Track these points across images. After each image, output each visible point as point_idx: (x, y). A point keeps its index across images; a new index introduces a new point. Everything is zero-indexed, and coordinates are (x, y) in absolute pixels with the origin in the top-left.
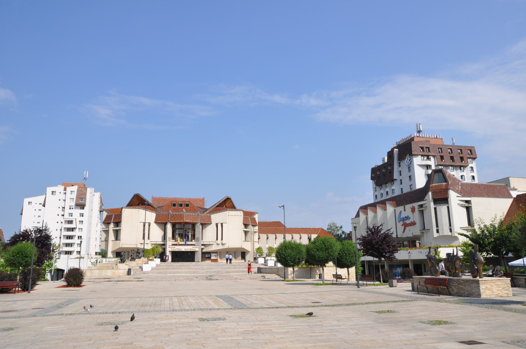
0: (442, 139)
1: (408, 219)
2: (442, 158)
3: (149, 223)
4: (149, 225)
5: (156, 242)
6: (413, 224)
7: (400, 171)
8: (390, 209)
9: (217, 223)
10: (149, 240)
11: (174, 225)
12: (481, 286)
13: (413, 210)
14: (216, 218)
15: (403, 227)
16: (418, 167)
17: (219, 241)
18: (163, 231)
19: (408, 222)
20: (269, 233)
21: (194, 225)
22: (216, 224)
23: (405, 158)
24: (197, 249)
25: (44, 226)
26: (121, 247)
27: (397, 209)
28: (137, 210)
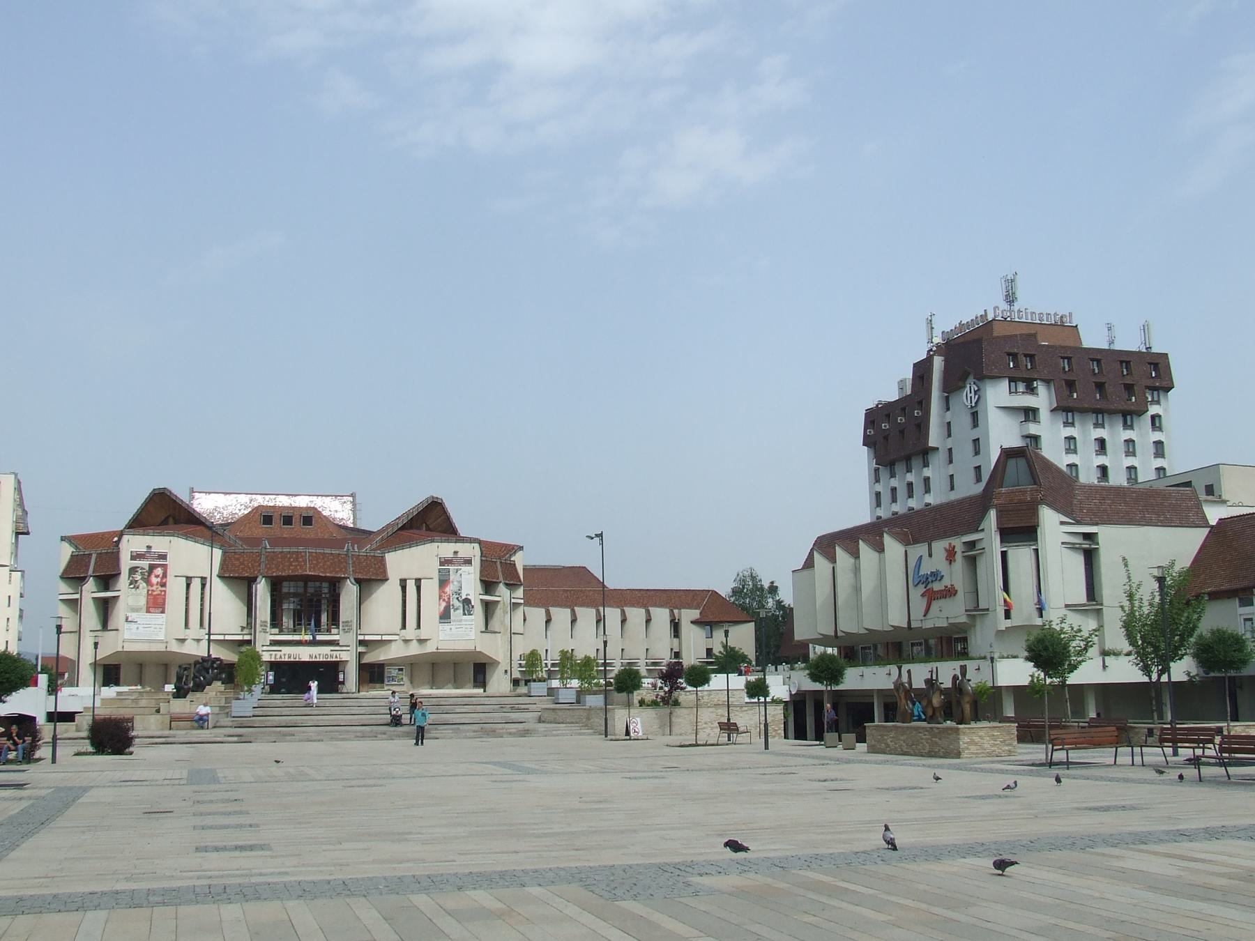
0: (1076, 326)
1: (939, 578)
2: (1071, 385)
3: (202, 578)
4: (203, 586)
5: (382, 635)
6: (950, 592)
7: (949, 424)
8: (893, 547)
9: (403, 577)
11: (276, 585)
12: (961, 737)
13: (951, 555)
14: (401, 562)
15: (925, 600)
16: (1000, 414)
17: (410, 632)
18: (243, 602)
19: (937, 586)
20: (553, 606)
21: (335, 585)
22: (400, 580)
23: (965, 387)
24: (348, 656)
25: (226, 636)
26: (120, 649)
27: (911, 549)
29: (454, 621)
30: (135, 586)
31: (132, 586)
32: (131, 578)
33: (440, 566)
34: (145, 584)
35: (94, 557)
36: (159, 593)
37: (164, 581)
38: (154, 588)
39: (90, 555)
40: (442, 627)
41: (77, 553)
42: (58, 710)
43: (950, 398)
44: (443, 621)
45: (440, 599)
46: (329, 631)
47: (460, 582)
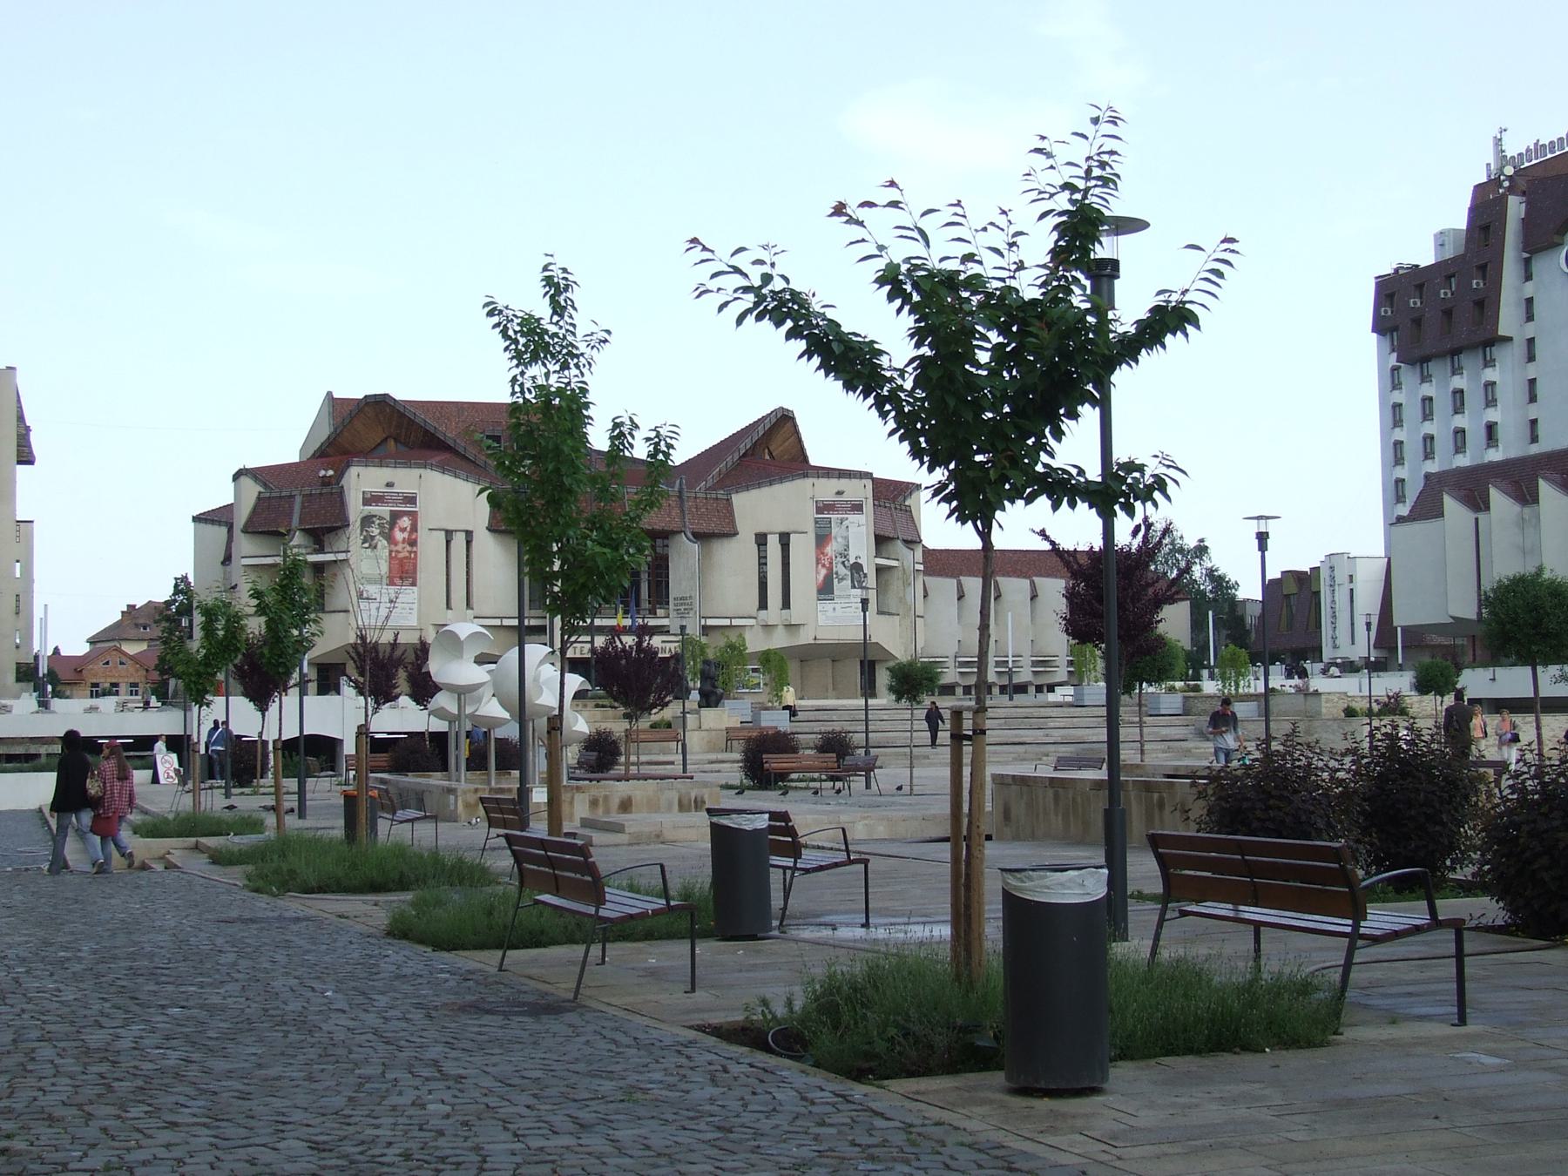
4: (469, 543)
5: (731, 618)
7: (1530, 301)
9: (763, 529)
10: (469, 611)
28: (416, 472)
29: (840, 597)
30: (370, 545)
31: (366, 545)
32: (365, 533)
33: (817, 513)
34: (385, 542)
35: (298, 499)
36: (407, 554)
37: (414, 537)
38: (399, 547)
39: (292, 497)
40: (821, 606)
41: (268, 495)
42: (1542, 694)
43: (1533, 262)
44: (823, 597)
45: (817, 564)
46: (653, 612)
47: (846, 538)
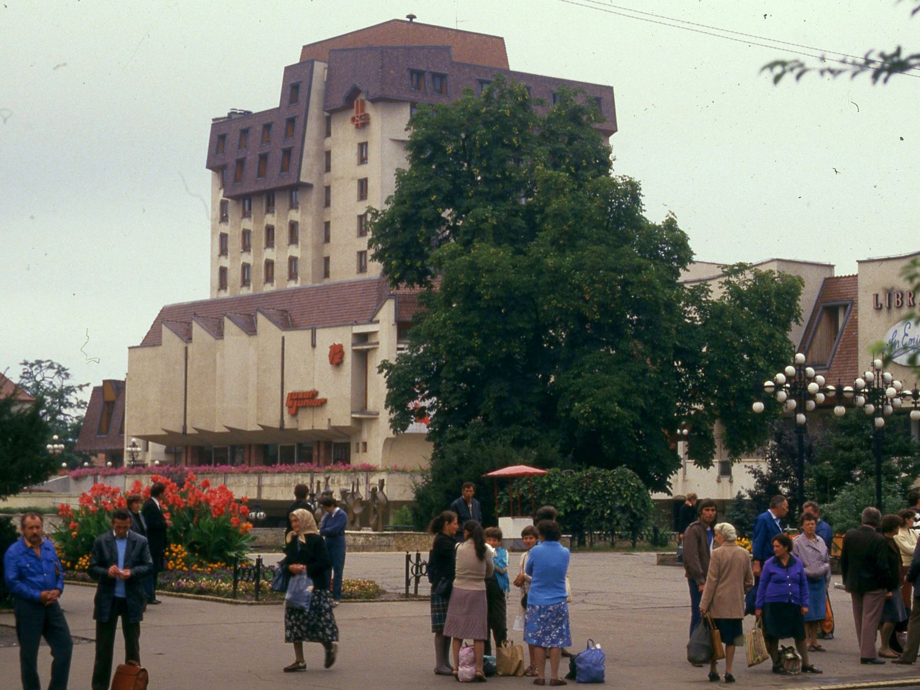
43: (332, 120)
